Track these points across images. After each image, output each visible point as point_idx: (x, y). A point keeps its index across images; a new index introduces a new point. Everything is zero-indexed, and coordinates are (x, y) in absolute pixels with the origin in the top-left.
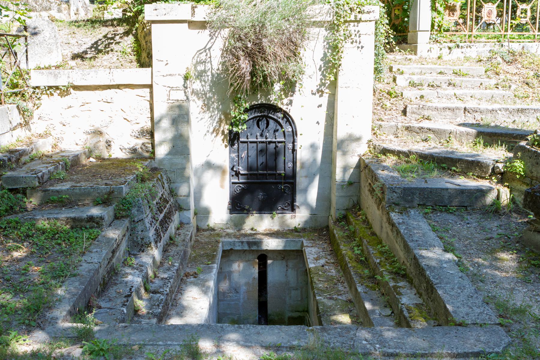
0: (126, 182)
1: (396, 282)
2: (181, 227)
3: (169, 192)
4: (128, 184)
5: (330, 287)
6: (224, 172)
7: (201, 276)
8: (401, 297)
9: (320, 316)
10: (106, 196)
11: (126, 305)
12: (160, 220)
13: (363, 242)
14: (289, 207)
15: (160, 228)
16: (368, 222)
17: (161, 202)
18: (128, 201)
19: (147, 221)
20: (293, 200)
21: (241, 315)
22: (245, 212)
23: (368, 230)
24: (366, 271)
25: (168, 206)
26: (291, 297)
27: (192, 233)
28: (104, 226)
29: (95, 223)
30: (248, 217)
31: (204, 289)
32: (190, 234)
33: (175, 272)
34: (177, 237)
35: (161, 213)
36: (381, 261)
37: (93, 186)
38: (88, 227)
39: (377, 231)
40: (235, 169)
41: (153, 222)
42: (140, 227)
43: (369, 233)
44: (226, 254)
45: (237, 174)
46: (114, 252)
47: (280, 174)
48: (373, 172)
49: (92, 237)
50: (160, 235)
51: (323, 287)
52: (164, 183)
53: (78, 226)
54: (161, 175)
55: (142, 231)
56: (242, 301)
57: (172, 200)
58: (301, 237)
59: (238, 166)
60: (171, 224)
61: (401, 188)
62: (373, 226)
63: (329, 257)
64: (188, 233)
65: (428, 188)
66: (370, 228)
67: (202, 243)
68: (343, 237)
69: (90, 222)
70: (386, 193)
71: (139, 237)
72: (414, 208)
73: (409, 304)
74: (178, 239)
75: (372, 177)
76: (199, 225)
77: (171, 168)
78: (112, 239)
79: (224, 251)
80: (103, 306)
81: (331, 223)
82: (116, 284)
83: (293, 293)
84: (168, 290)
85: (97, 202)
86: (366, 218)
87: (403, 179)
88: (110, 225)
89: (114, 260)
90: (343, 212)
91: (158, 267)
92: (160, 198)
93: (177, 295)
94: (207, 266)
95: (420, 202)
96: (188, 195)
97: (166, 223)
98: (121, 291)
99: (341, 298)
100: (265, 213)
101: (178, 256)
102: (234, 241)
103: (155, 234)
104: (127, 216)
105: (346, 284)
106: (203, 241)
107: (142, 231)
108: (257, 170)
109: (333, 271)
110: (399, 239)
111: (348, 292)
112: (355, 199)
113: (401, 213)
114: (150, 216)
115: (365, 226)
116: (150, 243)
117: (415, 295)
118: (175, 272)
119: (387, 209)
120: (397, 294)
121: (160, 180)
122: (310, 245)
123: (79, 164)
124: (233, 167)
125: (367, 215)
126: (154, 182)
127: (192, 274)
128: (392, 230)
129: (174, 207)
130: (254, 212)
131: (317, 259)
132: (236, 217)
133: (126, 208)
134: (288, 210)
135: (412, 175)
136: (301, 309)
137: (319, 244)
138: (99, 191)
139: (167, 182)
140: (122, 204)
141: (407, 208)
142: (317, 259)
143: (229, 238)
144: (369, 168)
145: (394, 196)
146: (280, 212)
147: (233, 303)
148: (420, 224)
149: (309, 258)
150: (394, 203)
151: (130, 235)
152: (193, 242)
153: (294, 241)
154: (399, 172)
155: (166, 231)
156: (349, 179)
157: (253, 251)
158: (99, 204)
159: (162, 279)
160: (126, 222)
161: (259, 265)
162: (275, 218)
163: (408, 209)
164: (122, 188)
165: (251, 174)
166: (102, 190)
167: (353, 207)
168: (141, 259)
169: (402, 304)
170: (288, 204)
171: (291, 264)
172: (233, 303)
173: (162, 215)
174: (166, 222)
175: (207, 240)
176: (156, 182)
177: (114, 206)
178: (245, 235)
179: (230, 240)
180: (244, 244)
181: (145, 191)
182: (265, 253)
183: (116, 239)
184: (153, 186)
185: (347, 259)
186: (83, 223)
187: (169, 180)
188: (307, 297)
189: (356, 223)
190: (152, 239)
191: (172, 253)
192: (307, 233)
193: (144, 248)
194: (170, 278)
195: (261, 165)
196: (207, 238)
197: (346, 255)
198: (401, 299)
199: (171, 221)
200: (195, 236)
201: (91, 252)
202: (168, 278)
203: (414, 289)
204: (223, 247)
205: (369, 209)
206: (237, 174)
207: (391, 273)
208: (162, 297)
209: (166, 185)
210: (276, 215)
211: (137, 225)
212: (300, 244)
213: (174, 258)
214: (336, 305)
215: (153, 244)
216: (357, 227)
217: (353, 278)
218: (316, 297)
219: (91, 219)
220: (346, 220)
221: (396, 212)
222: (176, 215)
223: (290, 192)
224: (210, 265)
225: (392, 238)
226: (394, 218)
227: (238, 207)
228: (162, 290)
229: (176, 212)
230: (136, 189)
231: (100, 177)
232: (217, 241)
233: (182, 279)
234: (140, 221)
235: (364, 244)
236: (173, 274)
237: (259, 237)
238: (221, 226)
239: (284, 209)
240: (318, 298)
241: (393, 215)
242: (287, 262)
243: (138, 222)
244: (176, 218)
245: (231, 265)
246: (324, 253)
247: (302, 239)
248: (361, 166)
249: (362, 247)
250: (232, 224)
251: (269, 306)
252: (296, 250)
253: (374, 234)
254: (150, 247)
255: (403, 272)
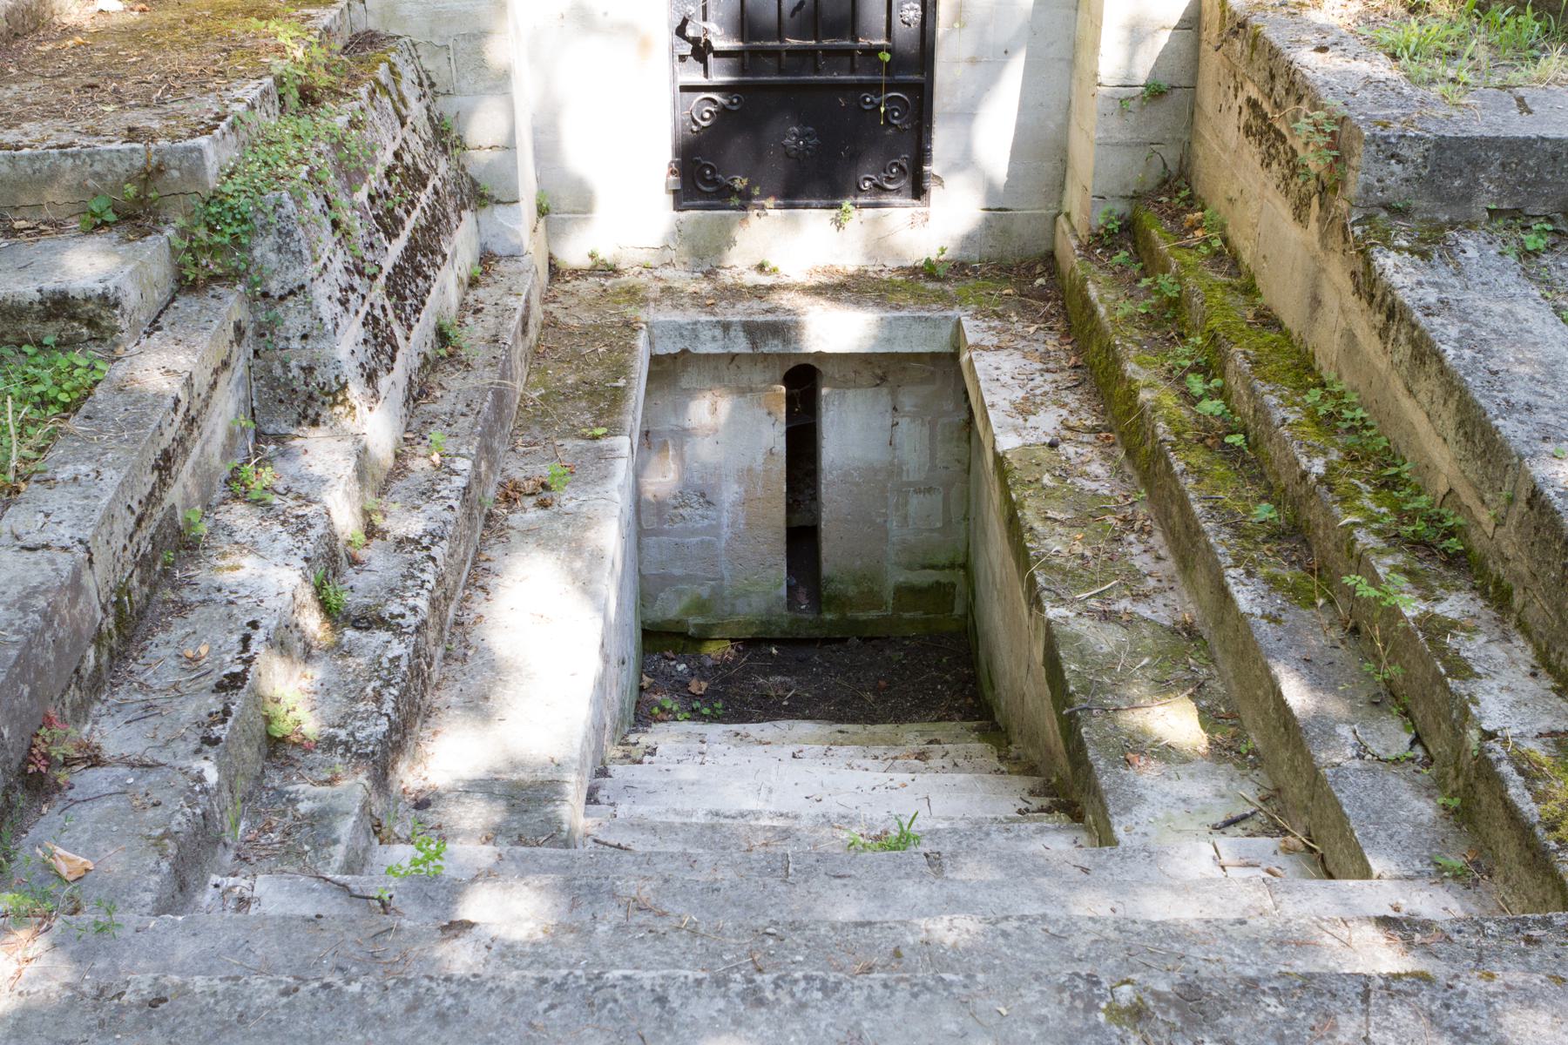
0: (220, 118)
1: (1428, 595)
2: (486, 273)
3: (428, 134)
4: (233, 127)
5: (1096, 556)
6: (645, 45)
7: (567, 499)
8: (1477, 688)
9: (1072, 715)
10: (131, 190)
11: (217, 741)
12: (387, 267)
13: (1226, 358)
14: (903, 182)
15: (388, 304)
16: (1236, 261)
17: (391, 191)
18: (231, 209)
19: (323, 294)
20: (921, 155)
21: (726, 583)
22: (735, 201)
23: (1241, 300)
24: (1264, 511)
25: (425, 197)
26: (905, 518)
27: (527, 301)
28: (125, 335)
29: (80, 321)
30: (744, 219)
31: (578, 564)
32: (519, 304)
33: (456, 504)
34: (469, 320)
35: (391, 235)
36: (1331, 468)
37: (71, 145)
38: (48, 340)
39: (1291, 314)
40: (690, 32)
41: (353, 289)
42: (293, 320)
43: (1250, 315)
44: (666, 370)
45: (701, 51)
46: (165, 464)
47: (873, 51)
48: (1274, 53)
49: (63, 397)
50: (390, 339)
51: (1065, 552)
52: (403, 100)
53: (8, 338)
54: (392, 69)
55: (304, 337)
56: (726, 533)
57: (442, 166)
58: (951, 302)
59: (705, 19)
60: (441, 275)
61: (1426, 140)
62: (1259, 282)
63: (1071, 399)
64: (511, 301)
65: (1543, 139)
66: (1250, 290)
67: (571, 334)
68: (1129, 319)
69: (57, 317)
70: (1354, 162)
71: (293, 363)
72: (1471, 225)
73: (1522, 735)
74: (473, 335)
75: (1272, 77)
76: (556, 254)
77: (431, 31)
78: (160, 396)
79: (655, 360)
80: (110, 749)
81: (1069, 250)
82: (183, 608)
83: (915, 501)
84: (422, 603)
85: (94, 215)
86: (1225, 240)
87: (1421, 92)
88: (155, 326)
89: (174, 495)
90: (1120, 207)
91: (382, 491)
92: (389, 172)
93: (466, 599)
94: (591, 444)
95: (1499, 201)
96: (509, 147)
97: (419, 274)
98: (203, 650)
99: (1147, 613)
100: (807, 207)
101: (471, 418)
102: (695, 323)
103: (366, 341)
104: (230, 277)
105: (1157, 539)
106: (575, 322)
107: (304, 337)
108: (780, 36)
109: (1096, 468)
110: (1427, 386)
111: (1171, 579)
112: (1171, 154)
113: (1424, 255)
114: (337, 265)
115: (1221, 278)
116: (344, 386)
117: (1534, 675)
118: (456, 504)
119: (1358, 230)
120: (1449, 674)
121: (385, 90)
122: (990, 339)
123: (48, 26)
124: (685, 22)
125: (1230, 231)
126: (356, 104)
127: (529, 486)
128: (1383, 334)
129: (452, 194)
130: (770, 202)
131: (1025, 409)
132: (698, 222)
133: (226, 240)
134: (898, 191)
135: (1451, 73)
136: (942, 559)
137: (1024, 338)
138: (98, 167)
139: (418, 91)
140: (208, 224)
141: (1441, 229)
142: (1025, 409)
143: (675, 307)
144: (1256, 37)
145: (1392, 174)
146: (868, 200)
147: (694, 540)
148: (1522, 310)
149: (993, 406)
150: (1387, 207)
151: (256, 352)
152: (533, 334)
153: (927, 319)
154: (1394, 57)
155: (417, 311)
156: (1153, 72)
157: (766, 356)
158: (105, 223)
159: (401, 543)
160: (231, 305)
161: (790, 400)
162: (847, 225)
163: (1449, 233)
164: (200, 150)
165: (754, 53)
166: (110, 162)
167: (1160, 186)
168: (306, 458)
169: (1491, 735)
170: (901, 168)
171: (908, 401)
172: (694, 540)
173: (397, 247)
174: (418, 271)
175: (589, 318)
176: (365, 102)
177: (169, 232)
178: (736, 293)
179: (678, 317)
180: (732, 333)
181: (312, 155)
182: (810, 361)
183: (177, 401)
184: (353, 124)
185: (1162, 429)
186: (29, 326)
187: (426, 83)
188: (966, 518)
189: (1183, 265)
190: (350, 371)
191: (444, 406)
192: (971, 282)
193: (317, 406)
194: (436, 537)
195: (793, 14)
196: (590, 307)
197: (1154, 411)
198: (1476, 703)
199: (439, 259)
200: (545, 301)
201: (49, 482)
202: (426, 541)
203: (1519, 641)
204: (651, 343)
205: (1239, 204)
206: (701, 51)
207: (1394, 540)
208: (398, 649)
209: (416, 110)
210: (855, 213)
211: (279, 309)
212: (946, 332)
213: (455, 429)
214: (1135, 655)
215: (356, 391)
216: (1190, 281)
217: (1200, 532)
218: (1042, 610)
219: (59, 306)
220: (1135, 242)
221: (1399, 249)
222: (463, 225)
223: (907, 122)
224: (603, 443)
225: (1382, 364)
226: (1398, 280)
227: (706, 183)
228: (395, 608)
229: (463, 213)
230: (271, 143)
231: (115, 91)
232: (627, 324)
233: (490, 516)
234: (292, 292)
235: (1231, 366)
236: (448, 516)
237: (787, 300)
238: (644, 257)
239: (885, 190)
240: (1052, 612)
241: (1389, 263)
242: (893, 393)
243: (282, 298)
244: (462, 244)
245: (685, 407)
246: (1049, 377)
247: (956, 312)
248: (1206, 18)
249: (1223, 376)
250: (684, 248)
251: (826, 549)
252: (933, 353)
253: (1268, 319)
254: (343, 403)
255: (1454, 544)
